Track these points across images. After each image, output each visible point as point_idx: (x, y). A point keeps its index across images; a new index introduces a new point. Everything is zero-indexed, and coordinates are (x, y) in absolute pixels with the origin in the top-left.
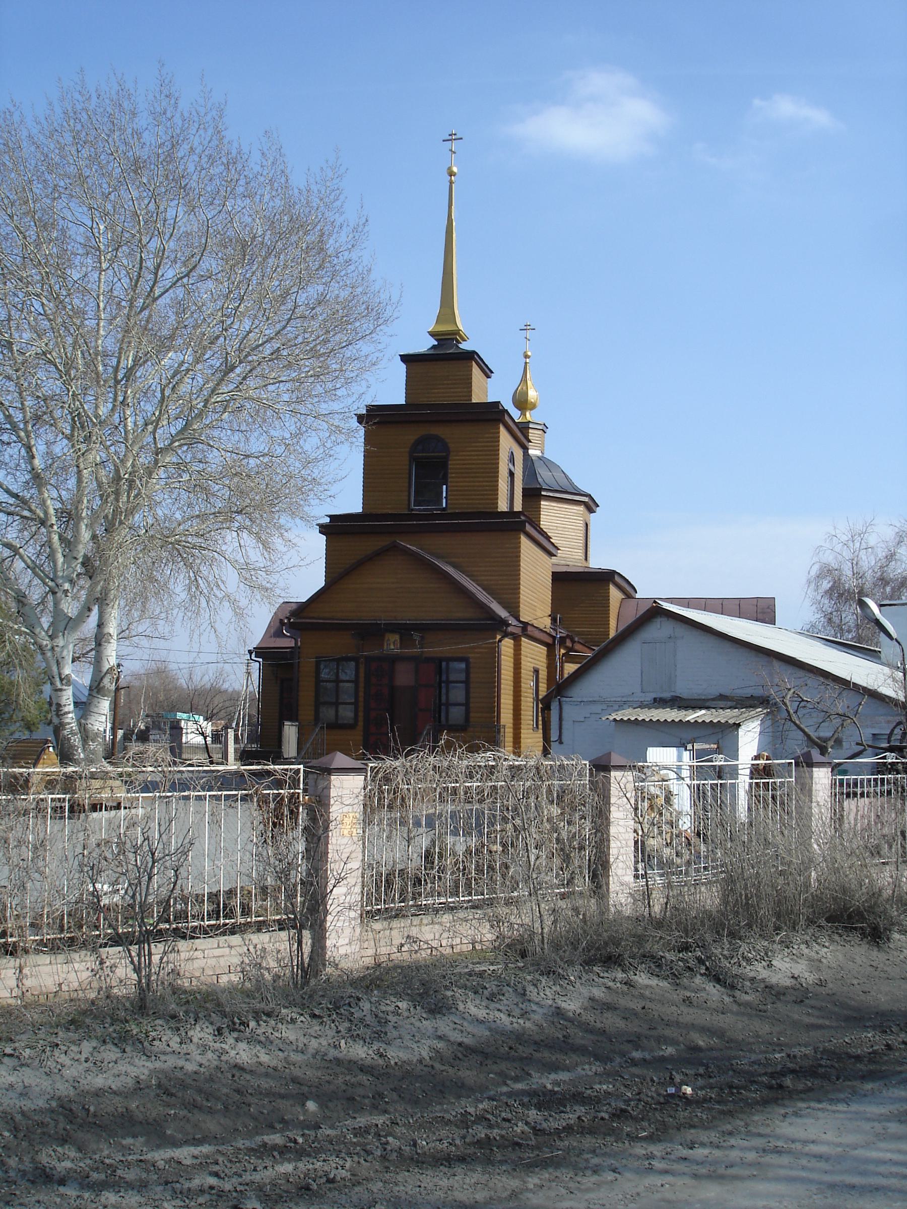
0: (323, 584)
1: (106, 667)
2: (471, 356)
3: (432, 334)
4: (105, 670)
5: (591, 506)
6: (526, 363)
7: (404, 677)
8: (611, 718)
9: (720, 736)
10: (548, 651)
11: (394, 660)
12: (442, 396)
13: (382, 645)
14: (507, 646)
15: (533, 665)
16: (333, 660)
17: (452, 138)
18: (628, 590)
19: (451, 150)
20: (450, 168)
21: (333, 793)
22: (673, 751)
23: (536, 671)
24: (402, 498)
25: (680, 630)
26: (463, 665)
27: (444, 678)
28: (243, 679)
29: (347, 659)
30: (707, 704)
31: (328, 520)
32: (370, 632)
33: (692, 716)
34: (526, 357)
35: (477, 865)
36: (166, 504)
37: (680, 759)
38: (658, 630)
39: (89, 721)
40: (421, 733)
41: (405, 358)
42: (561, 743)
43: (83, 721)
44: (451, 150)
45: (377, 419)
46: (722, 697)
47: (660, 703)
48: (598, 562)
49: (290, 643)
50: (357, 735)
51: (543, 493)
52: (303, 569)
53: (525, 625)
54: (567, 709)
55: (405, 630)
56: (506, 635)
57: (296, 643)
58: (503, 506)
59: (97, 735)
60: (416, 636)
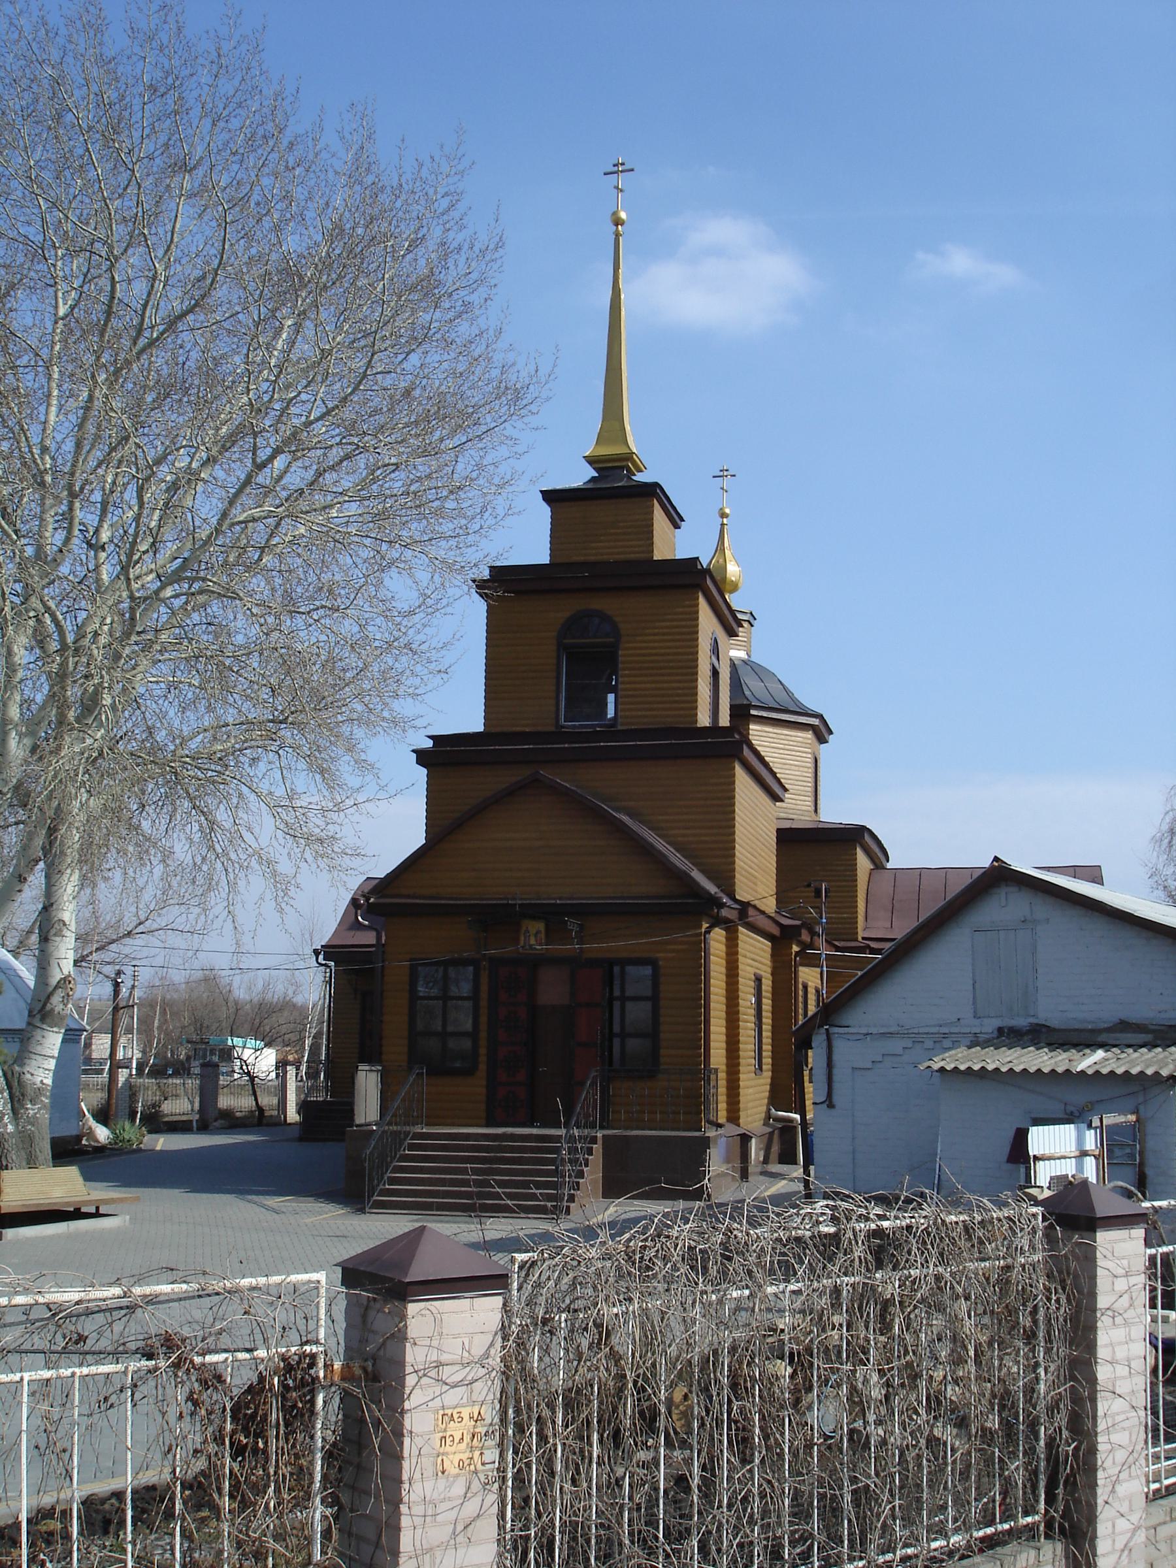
0: (417, 838)
1: (56, 976)
2: (653, 491)
3: (591, 461)
4: (54, 981)
5: (821, 732)
6: (723, 525)
7: (552, 990)
8: (936, 1067)
9: (1141, 1099)
10: (773, 948)
11: (536, 963)
12: (608, 549)
13: (517, 940)
14: (717, 939)
15: (752, 970)
16: (437, 963)
17: (618, 169)
18: (878, 854)
19: (617, 188)
20: (615, 214)
21: (414, 1356)
22: (1069, 1130)
23: (758, 980)
24: (545, 709)
25: (1043, 908)
26: (648, 971)
27: (617, 993)
28: (312, 989)
29: (464, 962)
30: (1102, 1038)
31: (429, 744)
32: (498, 918)
33: (1091, 1061)
34: (723, 515)
35: (796, 1495)
36: (164, 704)
37: (1080, 1140)
38: (1003, 908)
39: (26, 1069)
40: (583, 1084)
41: (550, 497)
42: (831, 1106)
43: (17, 1068)
44: (617, 188)
45: (506, 586)
46: (1124, 1026)
47: (1010, 1036)
48: (834, 813)
49: (369, 938)
50: (476, 1087)
51: (753, 712)
52: (390, 823)
53: (745, 906)
54: (839, 1046)
55: (553, 916)
56: (717, 922)
57: (379, 938)
58: (704, 719)
59: (39, 1091)
60: (573, 924)
